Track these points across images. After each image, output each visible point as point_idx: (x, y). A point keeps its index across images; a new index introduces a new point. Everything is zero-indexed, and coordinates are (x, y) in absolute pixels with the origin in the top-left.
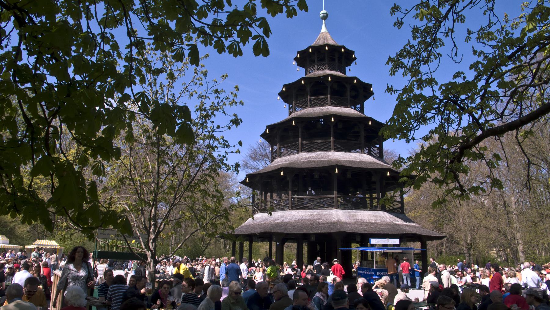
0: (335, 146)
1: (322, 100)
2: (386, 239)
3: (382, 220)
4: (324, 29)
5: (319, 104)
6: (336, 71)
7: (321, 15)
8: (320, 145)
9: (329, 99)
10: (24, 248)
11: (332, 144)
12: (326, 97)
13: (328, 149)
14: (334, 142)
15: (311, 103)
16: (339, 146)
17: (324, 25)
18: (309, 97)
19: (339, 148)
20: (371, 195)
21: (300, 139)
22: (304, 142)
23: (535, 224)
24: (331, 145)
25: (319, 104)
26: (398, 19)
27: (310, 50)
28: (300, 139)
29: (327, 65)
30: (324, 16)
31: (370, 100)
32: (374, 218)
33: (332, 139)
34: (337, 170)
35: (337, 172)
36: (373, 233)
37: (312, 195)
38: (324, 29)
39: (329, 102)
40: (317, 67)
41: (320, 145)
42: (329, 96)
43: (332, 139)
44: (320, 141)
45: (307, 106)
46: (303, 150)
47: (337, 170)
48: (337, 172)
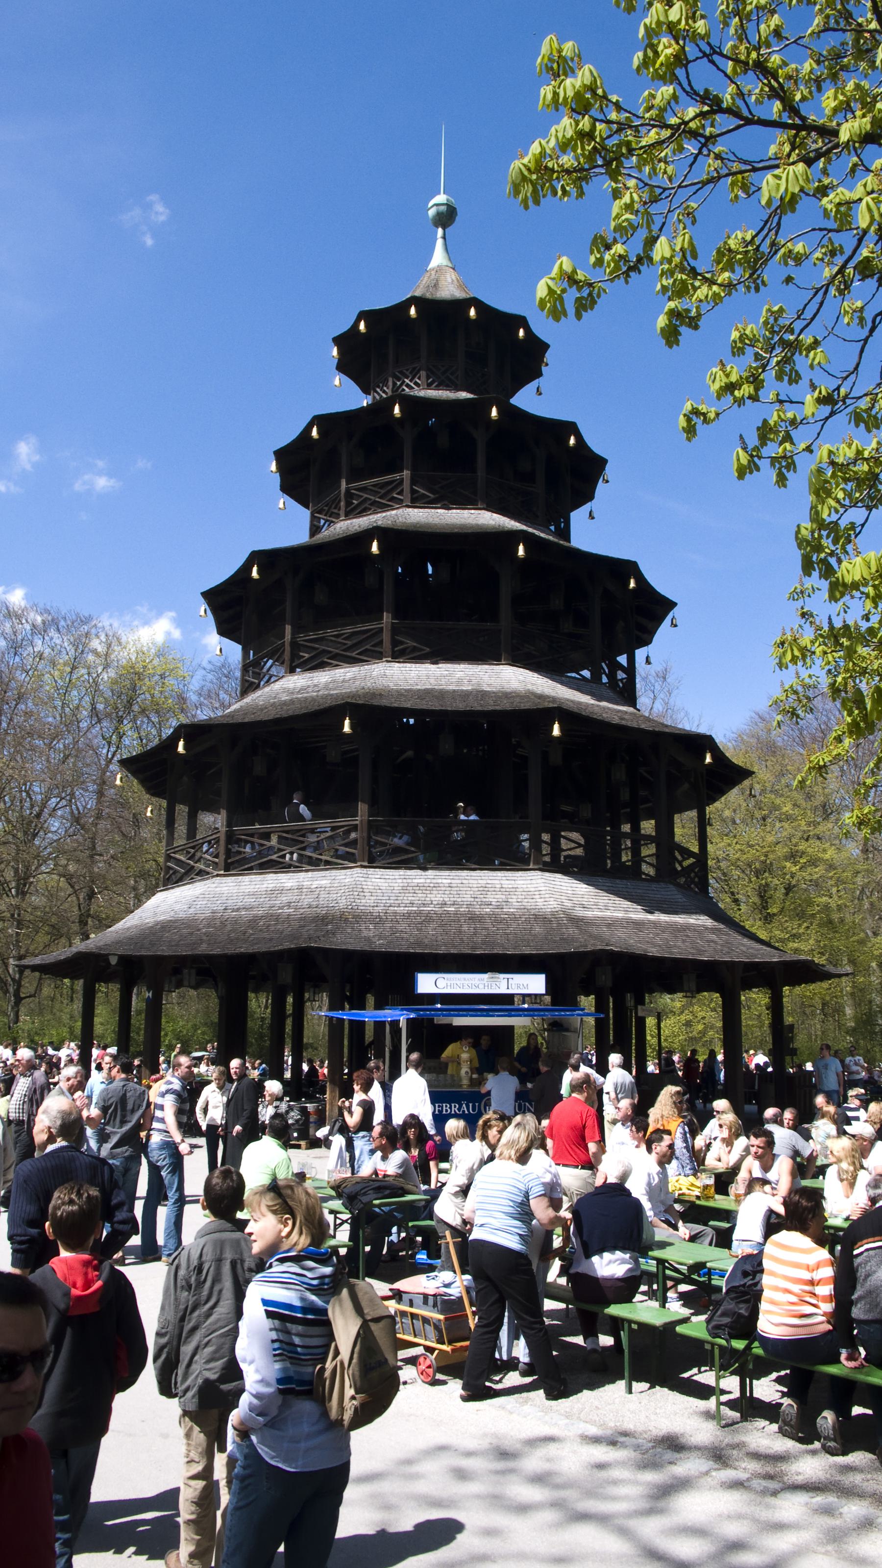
0: (395, 643)
1: (383, 491)
2: (485, 976)
3: (529, 904)
4: (439, 258)
5: (374, 503)
6: (457, 389)
7: (432, 213)
8: (349, 643)
9: (406, 485)
10: (560, 1253)
11: (386, 637)
12: (397, 476)
13: (376, 655)
14: (395, 630)
15: (348, 504)
16: (411, 643)
17: (440, 243)
18: (344, 484)
19: (414, 649)
20: (636, 828)
21: (288, 629)
22: (301, 638)
23: (719, 861)
24: (381, 642)
25: (374, 503)
26: (581, 194)
27: (413, 311)
28: (288, 629)
29: (423, 373)
30: (439, 214)
31: (608, 467)
32: (492, 898)
33: (387, 618)
34: (347, 722)
35: (347, 728)
36: (442, 950)
37: (301, 818)
38: (439, 258)
39: (407, 496)
40: (394, 384)
41: (349, 643)
42: (406, 473)
43: (387, 618)
44: (348, 630)
45: (338, 516)
46: (298, 666)
47: (347, 722)
48: (347, 728)
